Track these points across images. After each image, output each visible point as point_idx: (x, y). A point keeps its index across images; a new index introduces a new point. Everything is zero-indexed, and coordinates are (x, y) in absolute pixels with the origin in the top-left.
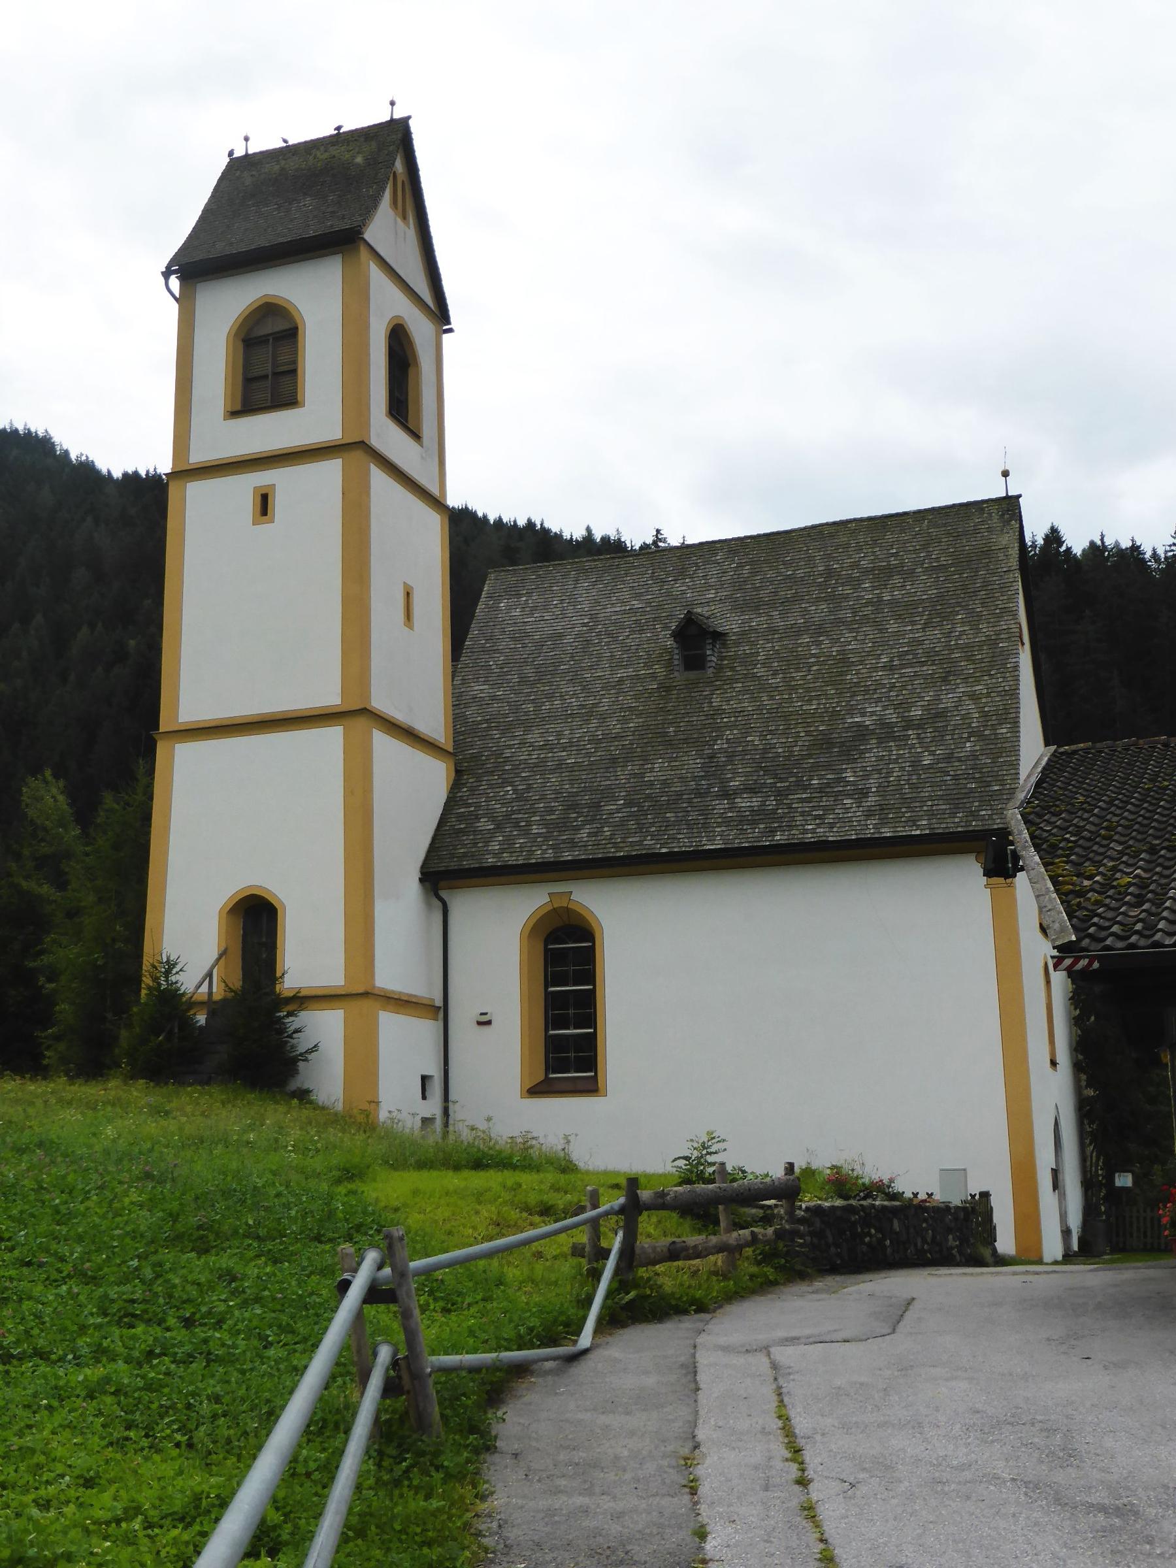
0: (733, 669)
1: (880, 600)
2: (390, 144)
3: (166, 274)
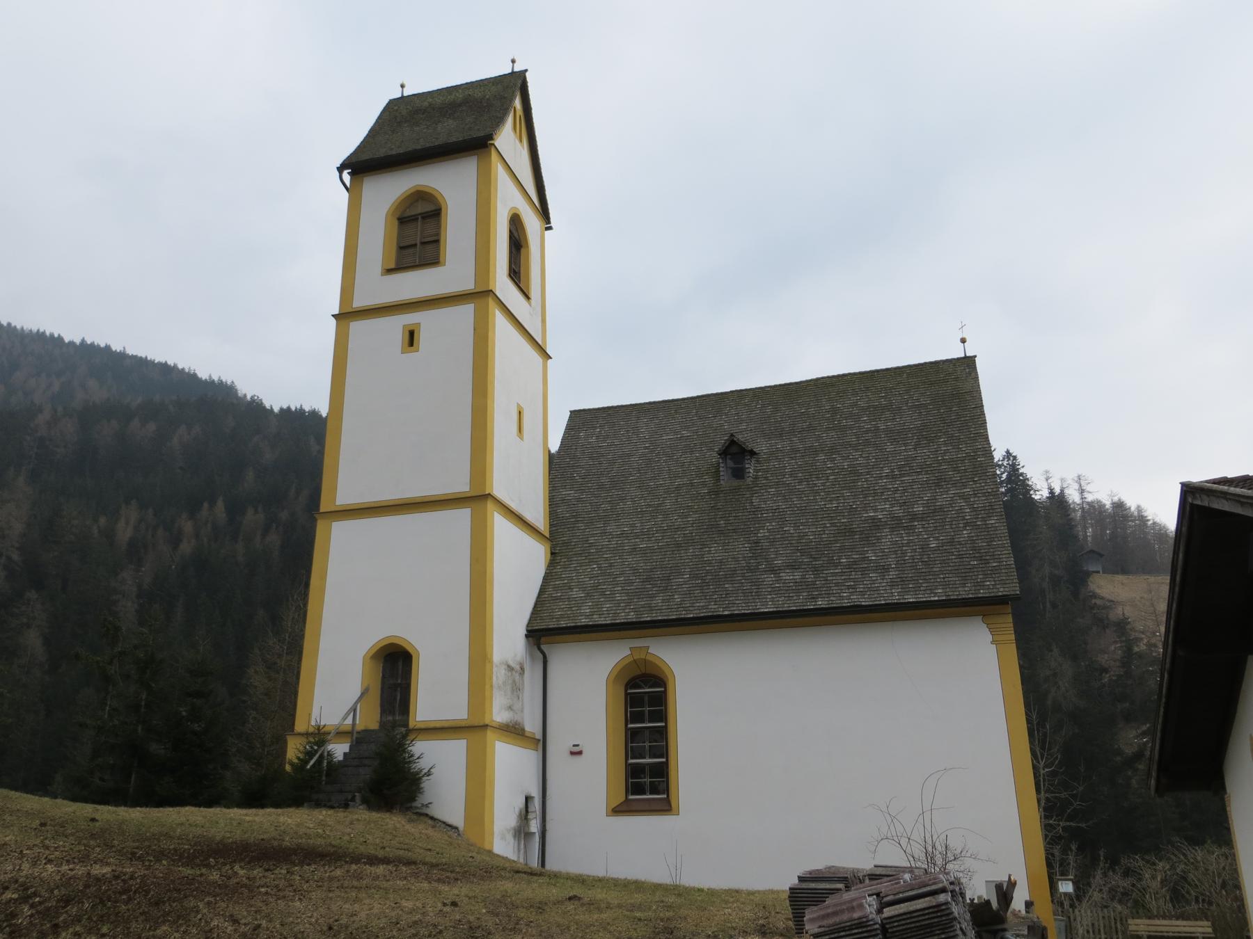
0: (766, 478)
1: (877, 429)
2: (504, 97)
3: (340, 170)
